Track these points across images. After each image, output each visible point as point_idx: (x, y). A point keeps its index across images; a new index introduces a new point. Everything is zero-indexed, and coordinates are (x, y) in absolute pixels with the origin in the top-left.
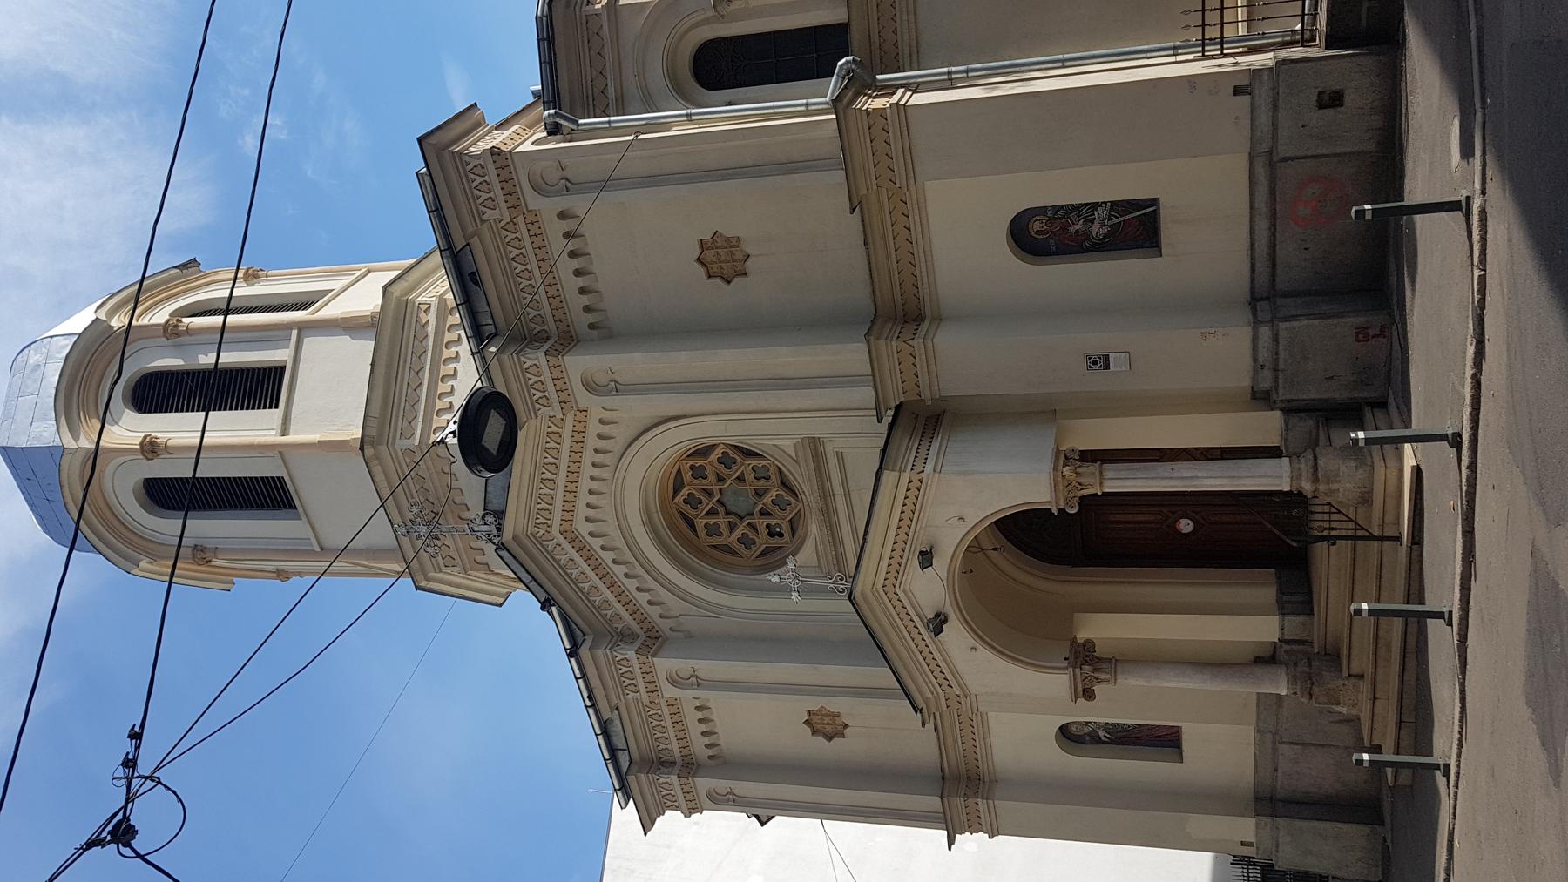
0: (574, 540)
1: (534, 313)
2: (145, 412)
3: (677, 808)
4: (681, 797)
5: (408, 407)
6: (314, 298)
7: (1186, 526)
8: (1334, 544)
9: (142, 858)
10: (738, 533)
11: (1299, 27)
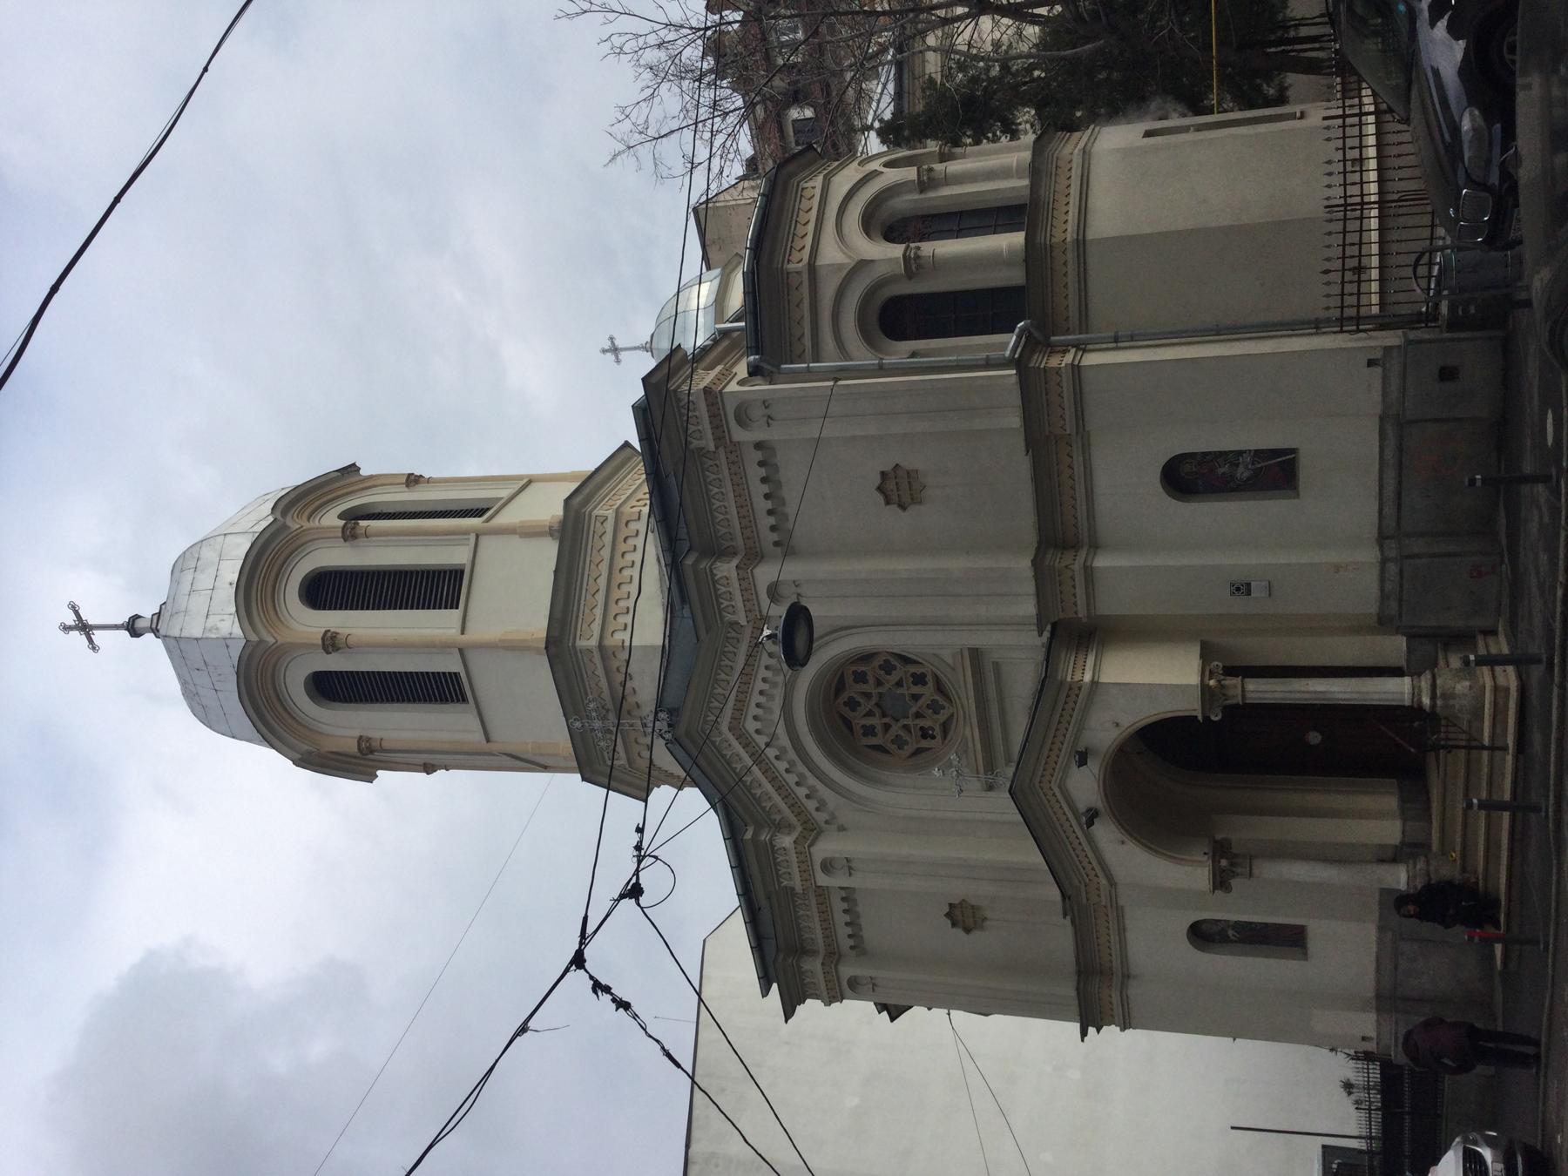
1: (725, 530)
2: (319, 609)
3: (817, 997)
4: (823, 986)
5: (587, 611)
7: (1314, 738)
8: (1450, 752)
9: (642, 908)
10: (869, 721)
11: (1424, 309)
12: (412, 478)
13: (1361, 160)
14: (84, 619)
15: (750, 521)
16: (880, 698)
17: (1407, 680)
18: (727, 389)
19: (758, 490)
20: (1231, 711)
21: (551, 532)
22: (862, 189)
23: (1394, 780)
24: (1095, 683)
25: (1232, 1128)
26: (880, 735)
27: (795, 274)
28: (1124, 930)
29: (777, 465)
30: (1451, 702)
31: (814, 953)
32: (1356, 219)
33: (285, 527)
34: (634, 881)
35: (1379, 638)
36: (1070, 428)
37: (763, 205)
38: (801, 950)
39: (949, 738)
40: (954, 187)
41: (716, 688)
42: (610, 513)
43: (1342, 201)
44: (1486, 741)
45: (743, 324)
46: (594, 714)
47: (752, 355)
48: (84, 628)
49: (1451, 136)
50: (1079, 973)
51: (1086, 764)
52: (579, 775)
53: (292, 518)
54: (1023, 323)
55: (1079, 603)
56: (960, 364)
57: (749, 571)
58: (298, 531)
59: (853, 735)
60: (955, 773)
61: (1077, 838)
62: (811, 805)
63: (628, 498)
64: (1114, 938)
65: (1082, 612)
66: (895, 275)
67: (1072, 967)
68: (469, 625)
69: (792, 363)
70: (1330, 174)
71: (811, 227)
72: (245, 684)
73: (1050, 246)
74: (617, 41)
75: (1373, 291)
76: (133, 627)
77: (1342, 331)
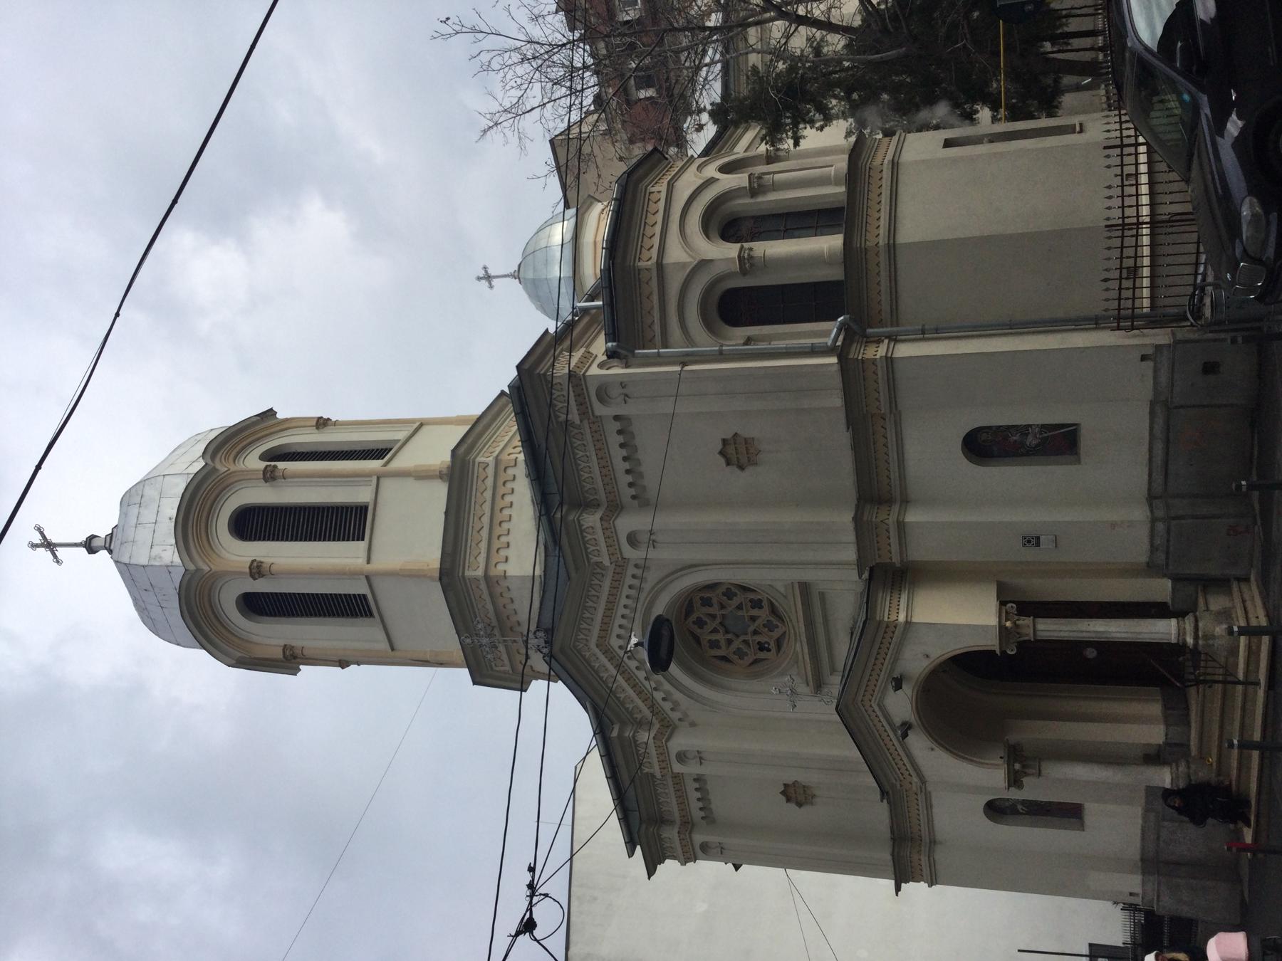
0: (607, 652)
3: (674, 858)
6: (389, 447)
8: (1210, 687)
9: (538, 941)
10: (714, 637)
12: (322, 421)
13: (1137, 174)
14: (48, 538)
15: (612, 532)
16: (723, 618)
17: (1173, 622)
18: (588, 373)
19: (617, 454)
20: (1022, 646)
21: (441, 476)
22: (705, 190)
23: (1158, 689)
24: (908, 623)
25: (1019, 951)
26: (724, 647)
27: (646, 271)
28: (931, 806)
29: (636, 446)
30: (1211, 642)
31: (672, 823)
32: (1132, 236)
33: (215, 470)
34: (528, 916)
35: (1148, 580)
36: (884, 409)
37: (616, 209)
38: (661, 820)
39: (781, 652)
40: (781, 192)
41: (585, 613)
42: (491, 460)
43: (1120, 222)
44: (1241, 676)
45: (601, 303)
46: (482, 633)
47: (610, 342)
48: (49, 545)
49: (1222, 192)
50: (893, 839)
51: (901, 688)
52: (467, 670)
53: (221, 461)
54: (842, 318)
55: (893, 551)
56: (789, 351)
57: (611, 522)
58: (225, 474)
59: (701, 648)
60: (790, 691)
61: (893, 745)
62: (667, 706)
63: (506, 445)
64: (923, 818)
65: (896, 559)
66: (732, 272)
67: (888, 835)
68: (373, 557)
69: (644, 348)
70: (1110, 197)
71: (658, 229)
72: (186, 604)
73: (866, 249)
74: (485, 57)
75: (1144, 285)
76: (90, 545)
77: (1118, 328)
